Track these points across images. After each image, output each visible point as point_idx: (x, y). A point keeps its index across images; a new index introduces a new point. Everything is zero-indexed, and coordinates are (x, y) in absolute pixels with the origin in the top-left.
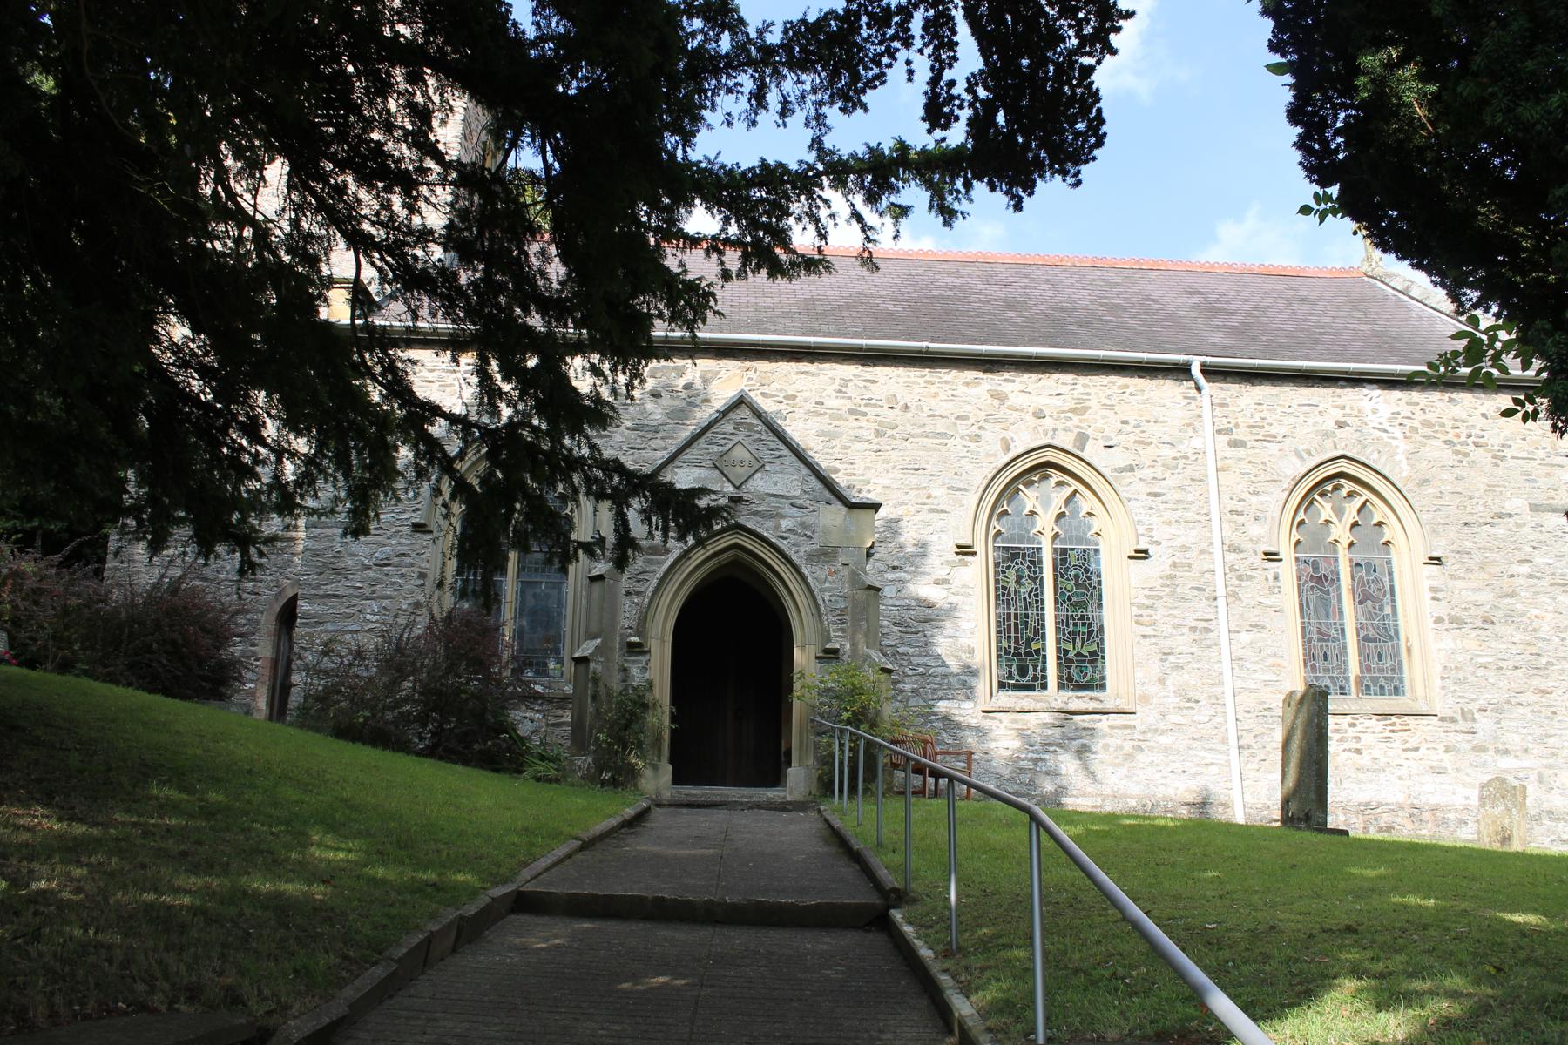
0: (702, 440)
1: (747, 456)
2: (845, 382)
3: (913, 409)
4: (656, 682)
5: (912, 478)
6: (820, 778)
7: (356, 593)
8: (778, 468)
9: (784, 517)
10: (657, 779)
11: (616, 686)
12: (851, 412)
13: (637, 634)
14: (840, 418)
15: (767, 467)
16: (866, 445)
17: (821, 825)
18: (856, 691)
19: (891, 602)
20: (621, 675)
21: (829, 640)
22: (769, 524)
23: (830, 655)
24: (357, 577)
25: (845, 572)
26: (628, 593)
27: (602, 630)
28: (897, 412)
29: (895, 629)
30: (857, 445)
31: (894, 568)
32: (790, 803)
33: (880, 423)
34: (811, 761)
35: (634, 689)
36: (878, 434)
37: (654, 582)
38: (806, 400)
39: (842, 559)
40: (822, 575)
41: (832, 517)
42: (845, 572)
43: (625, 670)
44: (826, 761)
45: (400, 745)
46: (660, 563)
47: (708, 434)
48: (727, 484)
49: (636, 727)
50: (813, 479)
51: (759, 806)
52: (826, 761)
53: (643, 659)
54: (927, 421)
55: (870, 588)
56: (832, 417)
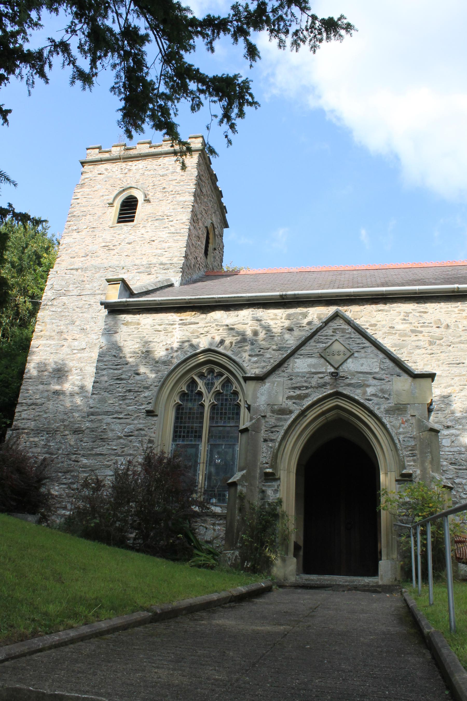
0: (312, 341)
1: (342, 348)
2: (407, 314)
3: (452, 327)
4: (284, 500)
5: (455, 369)
6: (402, 568)
7: (113, 452)
8: (363, 355)
9: (368, 386)
10: (285, 567)
11: (257, 502)
12: (413, 331)
13: (271, 467)
14: (405, 335)
15: (356, 355)
16: (423, 351)
17: (400, 604)
18: (425, 501)
19: (447, 449)
20: (260, 496)
21: (404, 468)
22: (359, 391)
23: (405, 478)
24: (114, 443)
25: (413, 421)
26: (265, 441)
27: (250, 465)
28: (442, 329)
29: (451, 467)
30: (418, 351)
31: (448, 427)
32: (379, 586)
33: (432, 337)
34: (395, 556)
35: (269, 504)
36: (431, 343)
37: (282, 432)
38: (383, 326)
39: (411, 411)
40: (397, 423)
41: (402, 384)
42: (413, 421)
43: (263, 492)
44: (406, 555)
45: (121, 543)
46: (286, 420)
47: (316, 337)
48: (329, 367)
49: (269, 530)
50: (387, 361)
51: (356, 588)
52: (406, 555)
53: (275, 484)
54: (462, 333)
55: (432, 430)
56: (400, 335)
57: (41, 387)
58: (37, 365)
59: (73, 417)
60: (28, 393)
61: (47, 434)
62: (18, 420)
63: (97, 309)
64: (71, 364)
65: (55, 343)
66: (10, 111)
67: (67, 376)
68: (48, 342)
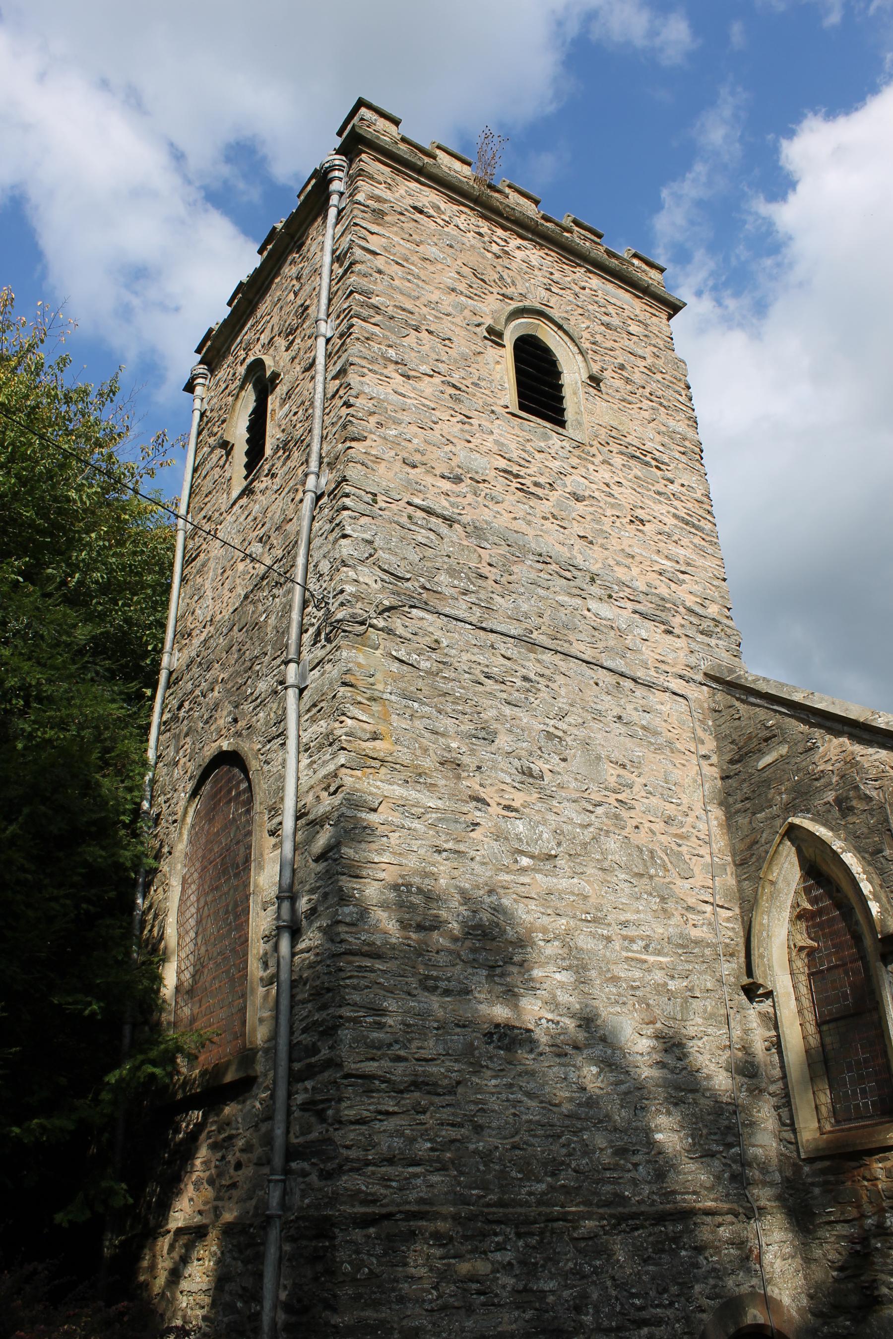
57: (435, 1004)
58: (392, 895)
59: (587, 1150)
60: (380, 1026)
61: (519, 1235)
62: (368, 1163)
63: (652, 673)
64: (527, 914)
65: (440, 804)
67: (521, 964)
68: (412, 794)
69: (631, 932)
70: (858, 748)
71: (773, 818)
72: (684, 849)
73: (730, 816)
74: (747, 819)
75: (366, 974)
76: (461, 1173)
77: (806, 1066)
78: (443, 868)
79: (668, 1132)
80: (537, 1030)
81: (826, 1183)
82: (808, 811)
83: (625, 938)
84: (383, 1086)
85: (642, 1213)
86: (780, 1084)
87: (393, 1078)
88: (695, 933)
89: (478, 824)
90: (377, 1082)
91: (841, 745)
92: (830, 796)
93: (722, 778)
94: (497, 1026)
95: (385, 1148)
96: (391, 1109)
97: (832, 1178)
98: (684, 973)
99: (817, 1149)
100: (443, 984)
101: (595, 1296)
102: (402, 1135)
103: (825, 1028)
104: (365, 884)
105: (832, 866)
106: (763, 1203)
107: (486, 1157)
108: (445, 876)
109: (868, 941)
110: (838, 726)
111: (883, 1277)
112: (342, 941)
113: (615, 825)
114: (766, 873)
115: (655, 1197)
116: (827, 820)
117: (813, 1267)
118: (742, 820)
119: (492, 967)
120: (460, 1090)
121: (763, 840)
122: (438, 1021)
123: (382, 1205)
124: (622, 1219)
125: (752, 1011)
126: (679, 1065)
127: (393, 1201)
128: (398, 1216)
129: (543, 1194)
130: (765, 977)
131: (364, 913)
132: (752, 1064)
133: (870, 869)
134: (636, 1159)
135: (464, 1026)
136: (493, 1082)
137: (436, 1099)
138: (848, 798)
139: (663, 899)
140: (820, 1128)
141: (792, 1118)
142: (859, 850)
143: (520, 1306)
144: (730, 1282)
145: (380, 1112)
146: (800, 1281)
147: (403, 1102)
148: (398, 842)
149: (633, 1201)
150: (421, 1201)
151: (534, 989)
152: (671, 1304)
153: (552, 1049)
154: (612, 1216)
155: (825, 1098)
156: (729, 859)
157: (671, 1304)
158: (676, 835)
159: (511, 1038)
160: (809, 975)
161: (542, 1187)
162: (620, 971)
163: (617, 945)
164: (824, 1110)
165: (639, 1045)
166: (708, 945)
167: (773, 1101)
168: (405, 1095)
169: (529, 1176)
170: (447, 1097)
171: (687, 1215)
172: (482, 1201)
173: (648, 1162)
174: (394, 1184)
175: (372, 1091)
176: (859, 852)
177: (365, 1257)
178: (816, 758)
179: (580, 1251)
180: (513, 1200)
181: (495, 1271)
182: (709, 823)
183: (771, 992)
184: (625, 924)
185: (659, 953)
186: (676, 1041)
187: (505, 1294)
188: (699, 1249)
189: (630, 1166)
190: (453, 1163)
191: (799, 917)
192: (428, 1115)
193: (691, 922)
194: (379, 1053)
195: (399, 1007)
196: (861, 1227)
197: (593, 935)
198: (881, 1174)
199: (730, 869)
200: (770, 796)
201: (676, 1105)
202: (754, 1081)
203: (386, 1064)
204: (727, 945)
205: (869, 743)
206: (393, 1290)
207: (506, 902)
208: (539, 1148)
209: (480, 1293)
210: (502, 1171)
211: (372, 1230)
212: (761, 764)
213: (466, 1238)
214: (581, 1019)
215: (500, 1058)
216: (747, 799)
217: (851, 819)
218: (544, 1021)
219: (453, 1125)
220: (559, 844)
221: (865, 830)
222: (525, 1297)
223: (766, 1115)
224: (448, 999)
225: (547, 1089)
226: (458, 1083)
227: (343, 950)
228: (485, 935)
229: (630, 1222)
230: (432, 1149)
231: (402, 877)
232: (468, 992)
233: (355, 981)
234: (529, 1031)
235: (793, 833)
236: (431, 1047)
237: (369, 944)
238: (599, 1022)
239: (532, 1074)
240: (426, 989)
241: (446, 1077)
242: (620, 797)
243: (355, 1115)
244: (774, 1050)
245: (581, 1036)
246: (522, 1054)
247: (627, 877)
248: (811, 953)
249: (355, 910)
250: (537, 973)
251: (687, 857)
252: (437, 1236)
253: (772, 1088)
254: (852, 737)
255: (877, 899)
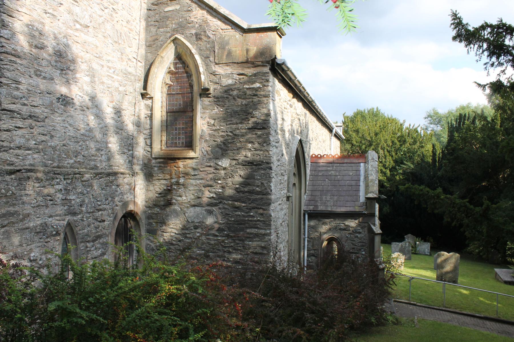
59: (88, 148)
60: (18, 89)
64: (76, 50)
66: (454, 38)
69: (110, 65)
70: (209, 17)
71: (167, 32)
72: (131, 35)
73: (148, 26)
74: (155, 30)
75: (13, 64)
76: (45, 154)
77: (160, 126)
78: (47, 21)
79: (114, 144)
80: (75, 99)
81: (160, 166)
82: (183, 34)
83: (108, 67)
84: (18, 116)
85: (103, 173)
86: (148, 131)
87: (22, 113)
88: (130, 70)
89: (62, 4)
90: (16, 114)
91: (203, 14)
92: (193, 31)
93: (147, 10)
94: (62, 95)
95: (18, 143)
96: (21, 126)
97: (163, 165)
98: (125, 85)
99: (159, 155)
100: (43, 74)
101: (87, 201)
102: (25, 137)
103: (168, 114)
104: (14, 21)
105: (188, 58)
106: (137, 171)
107: (54, 148)
108: (50, 27)
109: (196, 88)
110: (204, 6)
111: (174, 197)
112: (3, 46)
113: (111, 19)
114: (161, 53)
115: (106, 167)
116: (190, 40)
117: (149, 192)
118: (153, 29)
119: (62, 70)
120: (46, 120)
121: (160, 40)
122: (40, 90)
123: (15, 166)
124: (97, 174)
125: (142, 103)
126: (119, 119)
127: (20, 165)
128: (23, 171)
129: (73, 164)
130: (151, 92)
131: (14, 34)
132: (139, 122)
133: (203, 63)
134: (102, 153)
135: (50, 94)
136: (59, 118)
137: (38, 123)
138: (200, 34)
139: (122, 54)
140: (161, 148)
141: (151, 143)
142: (201, 55)
143: (63, 205)
144: (125, 197)
145: (16, 127)
146: (144, 197)
147: (25, 123)
148: (29, 3)
149: (100, 168)
150: (31, 165)
151: (76, 82)
152: (109, 204)
153: (80, 108)
154: (94, 173)
155: (164, 138)
156: (144, 43)
157: (109, 204)
158: (129, 29)
159: (65, 101)
160: (167, 94)
161: (72, 161)
162: (105, 80)
163: (105, 69)
164: (163, 142)
165: (108, 111)
166: (133, 75)
167: (144, 136)
168: (26, 121)
169: (68, 157)
170: (42, 123)
171: (115, 174)
172: (52, 165)
173: (106, 154)
174: (20, 157)
175: (13, 118)
176: (200, 56)
177: (11, 187)
178: (191, 15)
179: (83, 185)
180: (62, 166)
181: (56, 192)
182: (139, 26)
183: (152, 98)
184: (108, 61)
185: (118, 75)
186: (118, 110)
187: (59, 201)
188: (118, 186)
189: (100, 155)
190: (42, 150)
191: (169, 72)
192: (34, 129)
193: (129, 65)
194: (17, 101)
195: (26, 82)
196: (170, 182)
197: (98, 63)
198: (181, 166)
199: (144, 47)
200: (167, 23)
201: (116, 134)
202: (139, 128)
203: (19, 106)
204: (139, 76)
205: (215, 17)
206: (21, 199)
207: (70, 42)
208: (72, 146)
209: (51, 200)
210: (59, 154)
211: (13, 176)
212: (166, 10)
213: (47, 180)
214: (90, 97)
215: (62, 109)
216: (157, 21)
217: (199, 42)
218: (78, 96)
219: (43, 135)
220: (91, 22)
221: (205, 48)
222: (66, 201)
223: (141, 141)
224: (44, 81)
225: (77, 123)
226: (46, 117)
227: (3, 51)
228: (61, 55)
229: (100, 176)
230: (35, 144)
231: (30, 21)
232: (53, 79)
233: (8, 67)
234: (73, 99)
235: (175, 41)
236: (37, 101)
237: (15, 50)
238: (96, 99)
239: (72, 117)
240: (36, 75)
241: (42, 114)
242: (114, 7)
243: (6, 127)
244: (148, 118)
245: (90, 104)
246: (69, 108)
247: (112, 42)
248: (170, 86)
249: (9, 32)
250: (78, 75)
251: (132, 38)
252: (37, 179)
253: (145, 132)
254: (208, 12)
255: (204, 74)
